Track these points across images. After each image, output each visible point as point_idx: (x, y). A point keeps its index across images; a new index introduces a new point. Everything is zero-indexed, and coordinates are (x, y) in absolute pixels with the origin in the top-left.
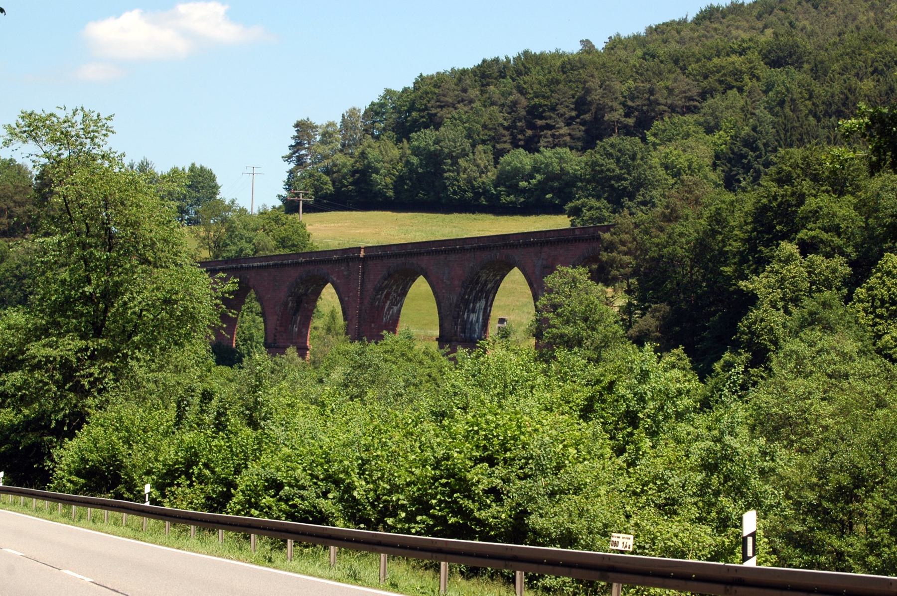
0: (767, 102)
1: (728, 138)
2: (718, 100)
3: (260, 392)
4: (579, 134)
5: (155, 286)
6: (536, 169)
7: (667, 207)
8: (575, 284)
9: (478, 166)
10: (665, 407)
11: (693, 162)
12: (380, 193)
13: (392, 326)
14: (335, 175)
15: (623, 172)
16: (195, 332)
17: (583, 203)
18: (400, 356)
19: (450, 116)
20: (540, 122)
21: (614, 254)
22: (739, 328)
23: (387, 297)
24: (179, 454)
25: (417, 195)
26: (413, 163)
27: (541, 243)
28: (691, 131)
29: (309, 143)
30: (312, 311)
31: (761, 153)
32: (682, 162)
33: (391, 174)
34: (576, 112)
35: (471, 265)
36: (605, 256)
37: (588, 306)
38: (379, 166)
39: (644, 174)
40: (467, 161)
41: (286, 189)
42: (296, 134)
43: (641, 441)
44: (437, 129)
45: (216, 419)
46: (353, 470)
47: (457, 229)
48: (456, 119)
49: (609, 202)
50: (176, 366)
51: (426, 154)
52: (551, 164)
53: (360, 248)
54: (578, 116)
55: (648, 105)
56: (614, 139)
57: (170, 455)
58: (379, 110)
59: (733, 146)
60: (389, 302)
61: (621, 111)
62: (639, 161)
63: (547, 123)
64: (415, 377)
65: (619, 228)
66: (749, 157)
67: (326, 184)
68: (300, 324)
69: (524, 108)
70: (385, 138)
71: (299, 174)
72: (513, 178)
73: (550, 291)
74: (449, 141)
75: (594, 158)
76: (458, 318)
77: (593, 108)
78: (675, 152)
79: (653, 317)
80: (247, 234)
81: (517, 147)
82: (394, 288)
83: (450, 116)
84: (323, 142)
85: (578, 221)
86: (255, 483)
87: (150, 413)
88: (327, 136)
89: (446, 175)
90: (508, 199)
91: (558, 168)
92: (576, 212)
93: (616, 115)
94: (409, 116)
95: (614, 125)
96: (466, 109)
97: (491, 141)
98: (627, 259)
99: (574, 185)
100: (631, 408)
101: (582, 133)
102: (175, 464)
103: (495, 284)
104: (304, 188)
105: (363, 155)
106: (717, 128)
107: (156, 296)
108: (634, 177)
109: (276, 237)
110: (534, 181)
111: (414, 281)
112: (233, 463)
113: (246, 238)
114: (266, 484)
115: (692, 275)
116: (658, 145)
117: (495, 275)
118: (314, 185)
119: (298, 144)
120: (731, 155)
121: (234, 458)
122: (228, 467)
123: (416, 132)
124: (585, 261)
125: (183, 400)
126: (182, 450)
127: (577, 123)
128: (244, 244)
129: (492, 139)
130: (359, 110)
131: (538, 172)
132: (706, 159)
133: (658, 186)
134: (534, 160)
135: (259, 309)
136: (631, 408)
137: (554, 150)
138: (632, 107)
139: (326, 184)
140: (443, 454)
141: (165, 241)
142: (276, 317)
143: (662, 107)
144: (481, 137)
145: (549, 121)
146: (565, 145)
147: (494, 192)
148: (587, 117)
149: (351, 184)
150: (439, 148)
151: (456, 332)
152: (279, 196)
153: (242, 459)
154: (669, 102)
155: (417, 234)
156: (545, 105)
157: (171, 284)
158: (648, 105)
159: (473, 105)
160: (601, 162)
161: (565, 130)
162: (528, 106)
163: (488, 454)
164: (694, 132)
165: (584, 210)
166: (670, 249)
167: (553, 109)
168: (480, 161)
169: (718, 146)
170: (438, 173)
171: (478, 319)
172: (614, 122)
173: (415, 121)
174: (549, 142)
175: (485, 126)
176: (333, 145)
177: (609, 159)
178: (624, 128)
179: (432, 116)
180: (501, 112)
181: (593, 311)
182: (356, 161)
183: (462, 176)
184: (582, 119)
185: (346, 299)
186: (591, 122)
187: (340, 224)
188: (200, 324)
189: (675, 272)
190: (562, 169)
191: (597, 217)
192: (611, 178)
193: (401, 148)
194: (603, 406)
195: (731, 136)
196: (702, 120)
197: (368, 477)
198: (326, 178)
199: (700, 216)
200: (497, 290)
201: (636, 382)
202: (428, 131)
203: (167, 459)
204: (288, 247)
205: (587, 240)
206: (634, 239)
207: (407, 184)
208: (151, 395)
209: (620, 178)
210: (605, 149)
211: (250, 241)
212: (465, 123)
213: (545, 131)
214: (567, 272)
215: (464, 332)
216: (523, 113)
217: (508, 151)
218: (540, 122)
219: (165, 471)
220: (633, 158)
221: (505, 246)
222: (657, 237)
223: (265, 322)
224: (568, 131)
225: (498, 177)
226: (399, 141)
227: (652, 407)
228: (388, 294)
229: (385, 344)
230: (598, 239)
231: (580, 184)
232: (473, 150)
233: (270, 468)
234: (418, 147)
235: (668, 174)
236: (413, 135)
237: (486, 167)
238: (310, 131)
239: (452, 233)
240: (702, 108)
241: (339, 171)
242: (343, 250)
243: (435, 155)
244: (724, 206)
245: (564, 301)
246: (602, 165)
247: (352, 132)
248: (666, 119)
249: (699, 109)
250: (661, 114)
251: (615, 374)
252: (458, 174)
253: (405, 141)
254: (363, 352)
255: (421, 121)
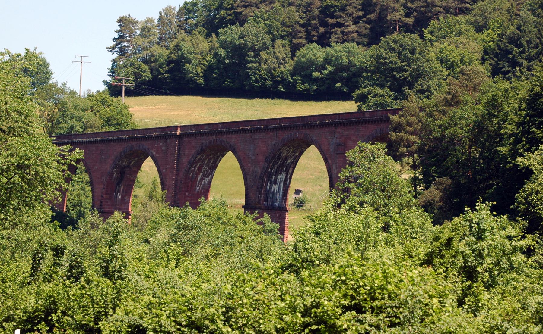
0: (530, 5)
1: (496, 36)
2: (487, 2)
3: (116, 246)
4: (365, 31)
5: (9, 152)
6: (327, 61)
7: (449, 93)
8: (374, 158)
9: (277, 58)
10: (501, 263)
11: (464, 57)
12: (192, 80)
13: (205, 192)
14: (153, 64)
15: (404, 64)
16: (44, 194)
17: (368, 91)
18: (216, 220)
19: (253, 14)
20: (331, 21)
21: (402, 134)
22: (517, 199)
23: (200, 169)
24: (39, 302)
25: (224, 83)
26: (221, 55)
27: (335, 124)
28: (462, 30)
29: (130, 36)
30: (133, 181)
31: (524, 49)
32: (455, 56)
33: (201, 64)
34: (363, 13)
35: (274, 143)
36: (393, 136)
37: (385, 177)
38: (191, 57)
39: (422, 66)
40: (267, 54)
41: (110, 75)
42: (119, 28)
43: (481, 294)
44: (242, 25)
45: (69, 271)
46: (219, 317)
47: (259, 112)
48: (258, 18)
49: (391, 90)
50: (27, 224)
51: (232, 47)
52: (341, 57)
53: (176, 127)
54: (364, 16)
55: (426, 7)
56: (396, 36)
57: (30, 304)
58: (191, 8)
59: (500, 43)
60: (201, 174)
61: (402, 12)
62: (418, 55)
63: (337, 22)
64: (232, 238)
65: (406, 111)
66: (514, 53)
67: (145, 72)
68: (123, 192)
69: (318, 8)
70: (197, 33)
71: (121, 63)
72: (307, 69)
73: (351, 164)
74: (252, 36)
75: (378, 52)
76: (262, 188)
77: (378, 9)
78: (450, 48)
79: (438, 189)
80: (77, 113)
81: (312, 42)
82: (206, 161)
83: (253, 14)
84: (142, 36)
85: (364, 106)
86: (119, 329)
87: (8, 266)
88: (146, 30)
89: (249, 65)
90: (303, 87)
91: (347, 60)
92: (362, 99)
93: (398, 15)
94: (217, 14)
95: (396, 24)
96: (267, 8)
97: (288, 37)
98: (412, 138)
99: (360, 76)
100: (469, 264)
101: (368, 31)
102: (35, 312)
103: (294, 159)
104: (126, 75)
105: (177, 47)
106: (486, 27)
107: (11, 162)
108: (413, 69)
109: (103, 117)
110: (325, 72)
111: (223, 156)
112: (94, 310)
113: (76, 117)
114: (130, 330)
115: (470, 152)
116: (436, 41)
117: (294, 152)
118: (135, 74)
119: (121, 37)
120: (498, 51)
121: (95, 306)
122: (88, 315)
123: (224, 28)
124: (381, 138)
125: (38, 253)
126: (42, 299)
127: (363, 21)
128: (74, 122)
129: (290, 34)
130: (174, 9)
131: (329, 64)
132: (476, 54)
133: (435, 76)
134: (326, 54)
135: (88, 179)
136: (469, 264)
137: (343, 45)
138: (412, 8)
139: (145, 72)
140: (312, 302)
141: (19, 112)
142: (102, 186)
143: (438, 9)
144: (280, 33)
145: (338, 20)
146: (353, 41)
147: (290, 80)
148: (372, 16)
149: (167, 72)
150: (243, 42)
151: (260, 200)
152: (104, 82)
153: (102, 307)
154: (444, 4)
155: (224, 116)
156: (337, 6)
157: (24, 151)
158: (426, 7)
159: (273, 5)
160: (385, 55)
161: (353, 28)
162: (321, 7)
163: (355, 304)
164: (466, 30)
165: (370, 97)
166: (452, 130)
167: (343, 9)
168: (279, 54)
169: (486, 42)
170: (243, 64)
171: (279, 189)
172: (395, 21)
173: (223, 18)
174: (339, 38)
175: (283, 24)
176: (152, 38)
177: (391, 53)
178: (404, 26)
179: (237, 14)
180: (297, 11)
181: (390, 182)
182: (171, 53)
183: (263, 66)
184: (368, 18)
185: (164, 171)
186: (375, 20)
187: (157, 107)
188: (49, 187)
189: (455, 150)
190: (350, 62)
191: (381, 103)
192: (393, 70)
193: (211, 42)
194: (442, 261)
195: (498, 34)
196: (472, 20)
197: (233, 324)
198: (145, 67)
199: (478, 102)
200: (296, 165)
201: (475, 240)
202: (233, 27)
203: (27, 307)
204: (112, 125)
205: (375, 122)
206: (420, 121)
207: (215, 73)
208: (4, 250)
209: (401, 70)
210: (388, 44)
211: (79, 119)
212: (266, 20)
213: (336, 29)
214: (367, 148)
215: (267, 201)
216: (317, 12)
217: (304, 46)
218: (331, 21)
219: (25, 318)
220: (413, 52)
221: (304, 126)
222: (441, 119)
223: (93, 190)
224: (356, 29)
225: (294, 68)
226: (208, 35)
227: (490, 262)
228: (201, 167)
229: (203, 209)
230: (388, 120)
231: (365, 75)
232: (273, 44)
233: (133, 315)
234: (225, 41)
235: (443, 67)
236: (221, 30)
237: (284, 59)
238: (131, 26)
239: (254, 115)
240: (473, 10)
241: (156, 61)
242: (162, 128)
243: (240, 48)
244: (500, 93)
245: (364, 173)
246: (386, 58)
247: (168, 27)
248: (441, 18)
249: (470, 11)
250: (437, 15)
251: (452, 231)
252: (260, 65)
253: (213, 35)
254: (186, 216)
255: (228, 18)
